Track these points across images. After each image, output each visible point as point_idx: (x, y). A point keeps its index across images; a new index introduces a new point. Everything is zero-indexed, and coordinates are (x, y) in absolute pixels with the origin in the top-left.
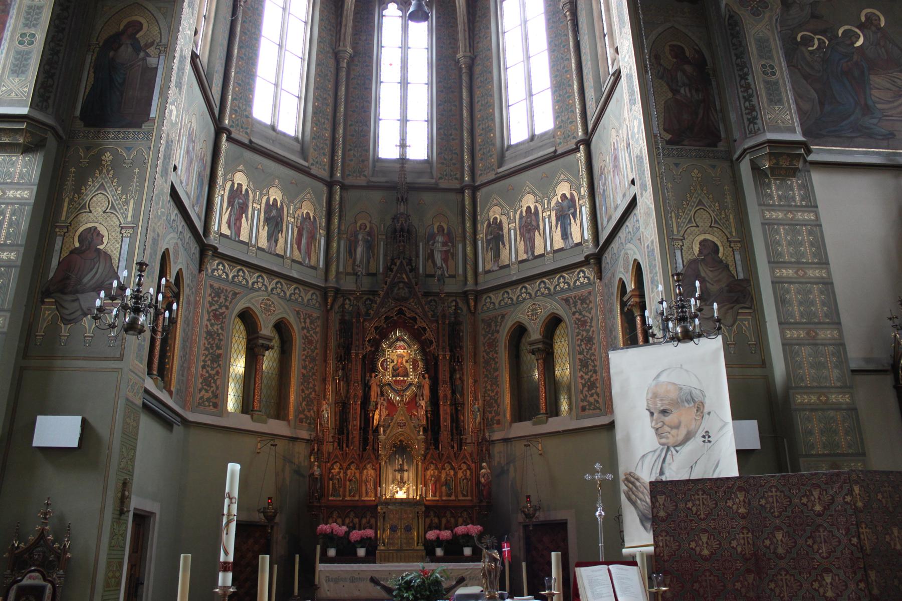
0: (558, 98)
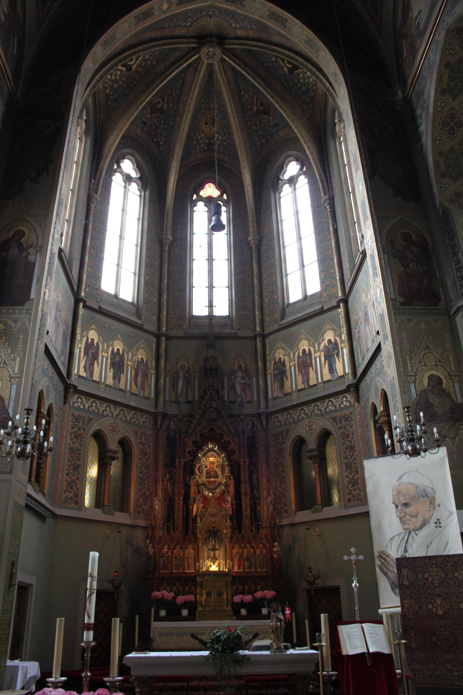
0: (323, 269)
